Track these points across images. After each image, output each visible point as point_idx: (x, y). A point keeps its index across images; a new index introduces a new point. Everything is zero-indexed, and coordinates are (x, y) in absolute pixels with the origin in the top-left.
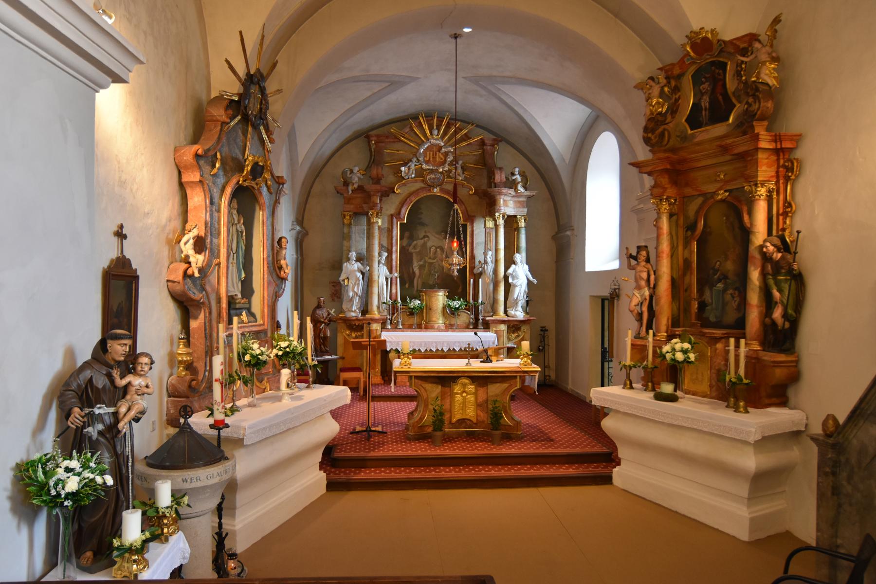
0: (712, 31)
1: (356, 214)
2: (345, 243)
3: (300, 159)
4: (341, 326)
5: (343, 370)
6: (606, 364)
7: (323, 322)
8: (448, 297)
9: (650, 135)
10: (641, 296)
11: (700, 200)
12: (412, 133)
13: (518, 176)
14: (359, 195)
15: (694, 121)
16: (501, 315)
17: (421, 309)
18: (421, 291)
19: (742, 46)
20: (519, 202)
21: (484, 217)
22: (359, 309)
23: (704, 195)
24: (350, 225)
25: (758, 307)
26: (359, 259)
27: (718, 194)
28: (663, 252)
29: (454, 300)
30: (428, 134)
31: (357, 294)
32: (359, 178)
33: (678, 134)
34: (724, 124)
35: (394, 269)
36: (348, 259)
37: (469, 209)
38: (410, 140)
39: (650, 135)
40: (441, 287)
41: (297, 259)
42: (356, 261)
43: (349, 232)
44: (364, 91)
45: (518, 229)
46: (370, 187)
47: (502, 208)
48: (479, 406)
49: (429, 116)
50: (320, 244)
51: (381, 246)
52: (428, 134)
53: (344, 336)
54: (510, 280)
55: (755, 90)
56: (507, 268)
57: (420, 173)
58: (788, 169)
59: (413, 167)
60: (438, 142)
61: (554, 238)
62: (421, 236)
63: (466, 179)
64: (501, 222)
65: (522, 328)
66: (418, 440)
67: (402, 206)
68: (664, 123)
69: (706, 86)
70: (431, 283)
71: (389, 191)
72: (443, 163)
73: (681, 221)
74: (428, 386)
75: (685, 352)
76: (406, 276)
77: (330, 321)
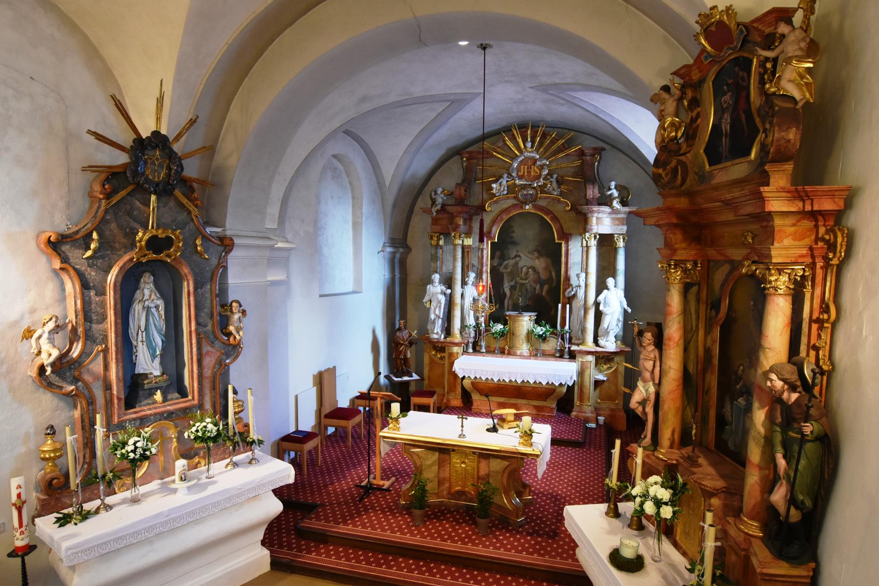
0: (728, 9)
3: (387, 183)
7: (402, 344)
9: (661, 171)
12: (506, 148)
15: (714, 155)
19: (768, 30)
20: (618, 219)
21: (581, 235)
27: (743, 266)
34: (743, 160)
37: (564, 226)
39: (661, 171)
40: (527, 309)
44: (428, 114)
45: (615, 250)
49: (522, 127)
54: (601, 308)
55: (779, 109)
56: (598, 292)
57: (512, 189)
63: (562, 194)
64: (593, 243)
65: (616, 359)
67: (493, 225)
68: (678, 153)
69: (727, 98)
72: (538, 177)
73: (704, 295)
75: (658, 503)
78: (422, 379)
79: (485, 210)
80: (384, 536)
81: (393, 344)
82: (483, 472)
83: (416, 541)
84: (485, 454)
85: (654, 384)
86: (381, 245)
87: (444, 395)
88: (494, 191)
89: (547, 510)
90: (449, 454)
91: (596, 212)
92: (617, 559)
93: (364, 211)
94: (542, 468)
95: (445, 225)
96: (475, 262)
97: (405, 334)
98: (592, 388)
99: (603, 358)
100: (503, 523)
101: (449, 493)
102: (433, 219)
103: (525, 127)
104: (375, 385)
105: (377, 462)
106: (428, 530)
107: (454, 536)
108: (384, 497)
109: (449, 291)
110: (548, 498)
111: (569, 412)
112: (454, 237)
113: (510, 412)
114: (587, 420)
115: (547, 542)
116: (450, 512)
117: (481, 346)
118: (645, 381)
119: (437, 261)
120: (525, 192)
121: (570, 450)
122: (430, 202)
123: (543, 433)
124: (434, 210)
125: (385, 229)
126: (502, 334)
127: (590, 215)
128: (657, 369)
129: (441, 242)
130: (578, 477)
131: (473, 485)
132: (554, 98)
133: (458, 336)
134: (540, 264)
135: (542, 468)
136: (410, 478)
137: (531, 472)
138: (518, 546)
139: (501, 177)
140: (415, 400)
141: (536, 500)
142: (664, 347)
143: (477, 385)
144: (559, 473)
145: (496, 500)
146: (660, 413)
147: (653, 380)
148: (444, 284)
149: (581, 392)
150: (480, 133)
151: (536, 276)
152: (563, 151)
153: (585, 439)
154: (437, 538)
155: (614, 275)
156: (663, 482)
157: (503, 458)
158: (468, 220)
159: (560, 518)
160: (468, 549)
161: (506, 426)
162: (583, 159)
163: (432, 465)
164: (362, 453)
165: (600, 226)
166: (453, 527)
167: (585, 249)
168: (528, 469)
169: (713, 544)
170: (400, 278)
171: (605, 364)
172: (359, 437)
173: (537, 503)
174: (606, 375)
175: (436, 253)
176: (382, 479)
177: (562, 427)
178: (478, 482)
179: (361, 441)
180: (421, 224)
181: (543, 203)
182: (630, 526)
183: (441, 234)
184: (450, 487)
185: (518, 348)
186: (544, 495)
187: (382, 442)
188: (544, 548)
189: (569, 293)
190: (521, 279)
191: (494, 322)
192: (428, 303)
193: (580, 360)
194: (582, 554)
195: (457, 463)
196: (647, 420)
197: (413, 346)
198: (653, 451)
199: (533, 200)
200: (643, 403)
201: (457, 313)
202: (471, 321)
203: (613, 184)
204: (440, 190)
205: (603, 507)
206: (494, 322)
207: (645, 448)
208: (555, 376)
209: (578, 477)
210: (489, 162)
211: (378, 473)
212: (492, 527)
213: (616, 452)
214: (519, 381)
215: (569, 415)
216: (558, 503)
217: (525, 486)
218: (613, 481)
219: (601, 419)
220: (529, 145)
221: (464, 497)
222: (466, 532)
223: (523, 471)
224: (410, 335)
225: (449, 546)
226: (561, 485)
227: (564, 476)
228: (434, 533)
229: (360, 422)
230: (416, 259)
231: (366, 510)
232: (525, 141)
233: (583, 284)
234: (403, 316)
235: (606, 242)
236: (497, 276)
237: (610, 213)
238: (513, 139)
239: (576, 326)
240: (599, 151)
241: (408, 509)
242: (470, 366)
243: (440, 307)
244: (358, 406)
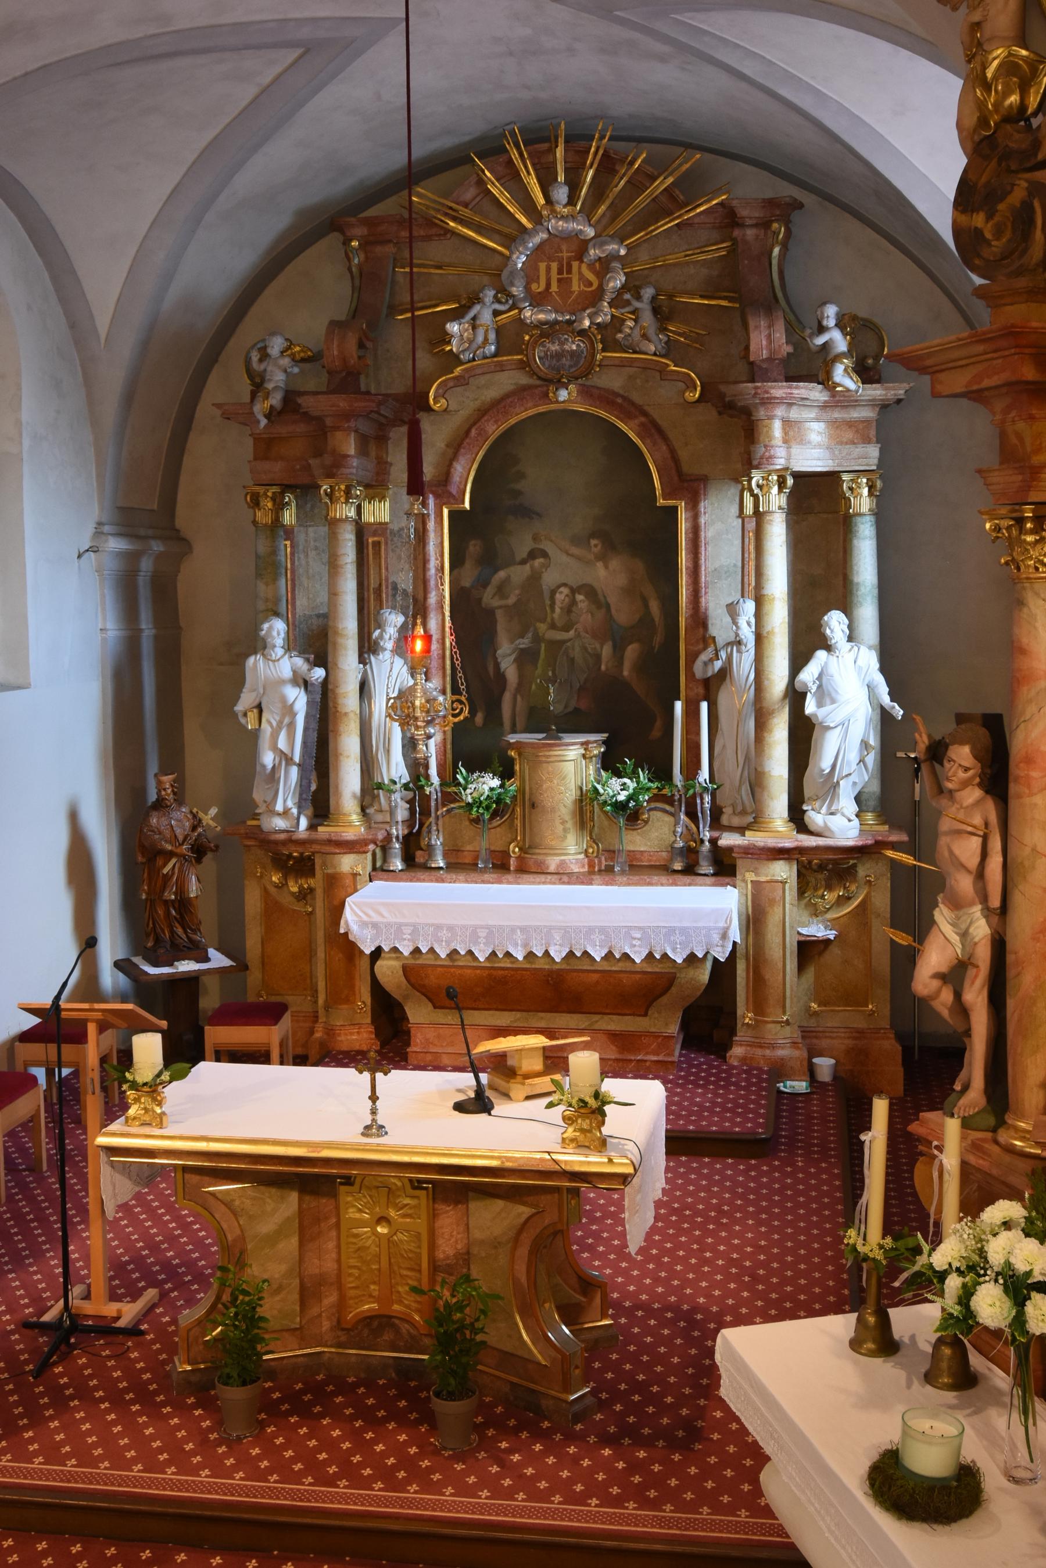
7: (171, 854)
9: (979, 220)
20: (850, 424)
21: (737, 480)
37: (683, 454)
39: (979, 220)
44: (228, 88)
45: (846, 523)
49: (538, 138)
52: (541, 200)
56: (798, 660)
57: (511, 338)
62: (522, 553)
63: (670, 349)
64: (776, 500)
65: (861, 872)
78: (242, 966)
79: (429, 409)
80: (123, 1481)
81: (140, 855)
82: (447, 1248)
83: (231, 1490)
84: (452, 1186)
85: (988, 912)
86: (90, 528)
87: (316, 1018)
88: (454, 346)
89: (663, 1360)
90: (334, 1195)
91: (781, 401)
92: (895, 1486)
93: (25, 416)
94: (638, 1221)
95: (297, 458)
96: (405, 580)
97: (178, 821)
98: (791, 964)
99: (823, 869)
100: (520, 1411)
101: (339, 1325)
102: (257, 439)
103: (547, 140)
104: (89, 986)
105: (94, 1243)
106: (271, 1451)
107: (362, 1465)
108: (120, 1355)
109: (319, 673)
110: (663, 1323)
111: (721, 1049)
112: (330, 496)
113: (525, 1045)
114: (779, 1071)
115: (665, 1462)
116: (343, 1388)
117: (430, 849)
118: (957, 904)
119: (275, 579)
120: (555, 347)
121: (728, 1167)
122: (246, 386)
123: (639, 1109)
124: (260, 408)
125: (100, 476)
126: (498, 808)
127: (762, 413)
128: (995, 862)
129: (289, 517)
130: (759, 1249)
131: (415, 1290)
132: (636, 35)
133: (355, 818)
134: (610, 575)
135: (638, 1221)
136: (205, 1285)
137: (607, 1242)
138: (571, 1481)
139: (475, 299)
140: (216, 1035)
141: (625, 1330)
142: (1013, 788)
143: (419, 971)
144: (699, 1241)
145: (493, 1335)
146: (1011, 1003)
147: (984, 897)
148: (302, 653)
149: (758, 981)
150: (398, 160)
151: (600, 614)
152: (668, 213)
153: (777, 1129)
154: (302, 1474)
155: (846, 607)
156: (1029, 1220)
157: (514, 1194)
158: (374, 441)
159: (705, 1376)
160: (410, 1503)
161: (518, 1090)
162: (733, 230)
163: (279, 1234)
164: (42, 1220)
165: (796, 450)
166: (356, 1436)
167: (751, 525)
168: (596, 1235)
170: (156, 638)
171: (829, 888)
172: (34, 1168)
173: (630, 1339)
174: (833, 924)
175: (274, 552)
176: (114, 1297)
177: (700, 1097)
178: (432, 1281)
179: (40, 1179)
180: (219, 460)
181: (611, 381)
182: (929, 1378)
183: (287, 488)
184: (342, 1305)
185: (552, 851)
186: (650, 1312)
187: (105, 1170)
188: (658, 1481)
189: (706, 665)
190: (553, 626)
191: (470, 770)
192: (252, 716)
193: (750, 876)
194: (779, 1486)
195: (363, 1224)
196: (968, 1033)
197: (208, 858)
198: (994, 1130)
199: (581, 371)
200: (955, 975)
201: (349, 744)
202: (395, 768)
203: (831, 312)
204: (276, 345)
205: (841, 1325)
206: (470, 770)
207: (966, 1124)
208: (671, 931)
209: (759, 1249)
210: (436, 251)
211: (98, 1275)
212: (486, 1425)
213: (876, 1140)
214: (558, 954)
215: (723, 1058)
216: (697, 1332)
217: (587, 1285)
218: (870, 1237)
219: (825, 1064)
220: (561, 194)
221: (387, 1336)
222: (399, 1450)
223: (580, 1241)
224: (197, 823)
225: (346, 1499)
226: (704, 1276)
227: (713, 1248)
228: (294, 1460)
229: (34, 1118)
230: (210, 573)
231: (60, 1403)
232: (547, 183)
233: (747, 633)
234: (173, 759)
235: (816, 499)
236: (472, 623)
237: (825, 407)
238: (511, 178)
239: (733, 771)
240: (783, 210)
241: (202, 1390)
242: (392, 913)
243: (291, 726)
244: (27, 1064)
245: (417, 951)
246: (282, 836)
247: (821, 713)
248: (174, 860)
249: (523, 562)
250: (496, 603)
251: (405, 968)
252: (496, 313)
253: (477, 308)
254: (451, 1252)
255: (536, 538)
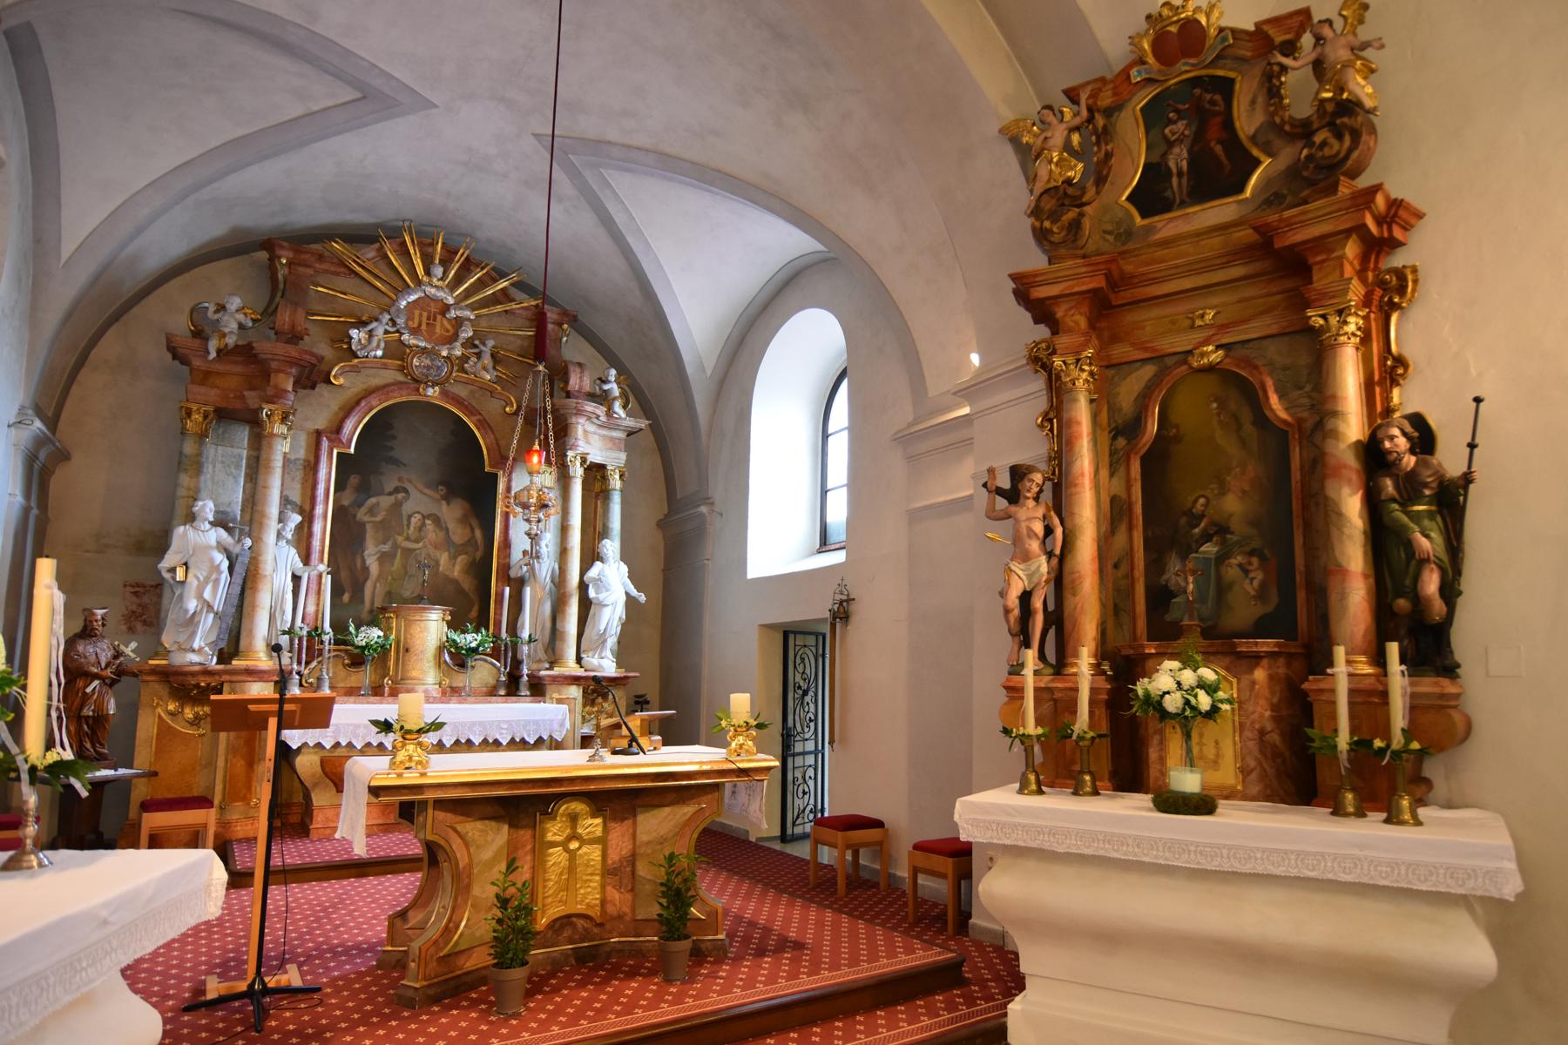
1: (224, 415)
2: (184, 479)
3: (67, 248)
4: (153, 690)
5: (148, 806)
6: (790, 760)
7: (96, 676)
8: (450, 625)
10: (1030, 576)
11: (1148, 371)
12: (382, 265)
13: (615, 386)
14: (239, 369)
16: (570, 667)
17: (383, 650)
18: (384, 610)
20: (612, 439)
22: (212, 644)
23: (1158, 358)
24: (203, 436)
25: (1366, 576)
26: (221, 522)
27: (1203, 355)
28: (1082, 475)
29: (464, 632)
30: (420, 270)
31: (210, 607)
32: (241, 326)
33: (1109, 227)
35: (315, 556)
36: (191, 518)
38: (376, 277)
39: (1047, 224)
40: (437, 599)
41: (26, 511)
42: (214, 524)
43: (199, 454)
46: (267, 347)
47: (581, 443)
48: (610, 872)
50: (98, 487)
51: (285, 501)
52: (420, 270)
53: (157, 714)
54: (592, 593)
56: (586, 566)
57: (397, 352)
58: (1390, 294)
59: (380, 332)
60: (441, 294)
61: (662, 524)
62: (389, 487)
63: (499, 380)
64: (577, 472)
66: (436, 1000)
70: (407, 594)
71: (313, 377)
72: (451, 340)
74: (473, 828)
76: (344, 575)
77: (121, 672)
86: (15, 411)
169: (1335, 670)
181: (461, 391)
190: (408, 539)
245: (338, 744)
246: (197, 668)
247: (601, 597)
248: (96, 683)
249: (390, 494)
250: (366, 519)
251: (323, 762)
252: (386, 332)
253: (374, 325)
254: (616, 858)
255: (400, 479)
